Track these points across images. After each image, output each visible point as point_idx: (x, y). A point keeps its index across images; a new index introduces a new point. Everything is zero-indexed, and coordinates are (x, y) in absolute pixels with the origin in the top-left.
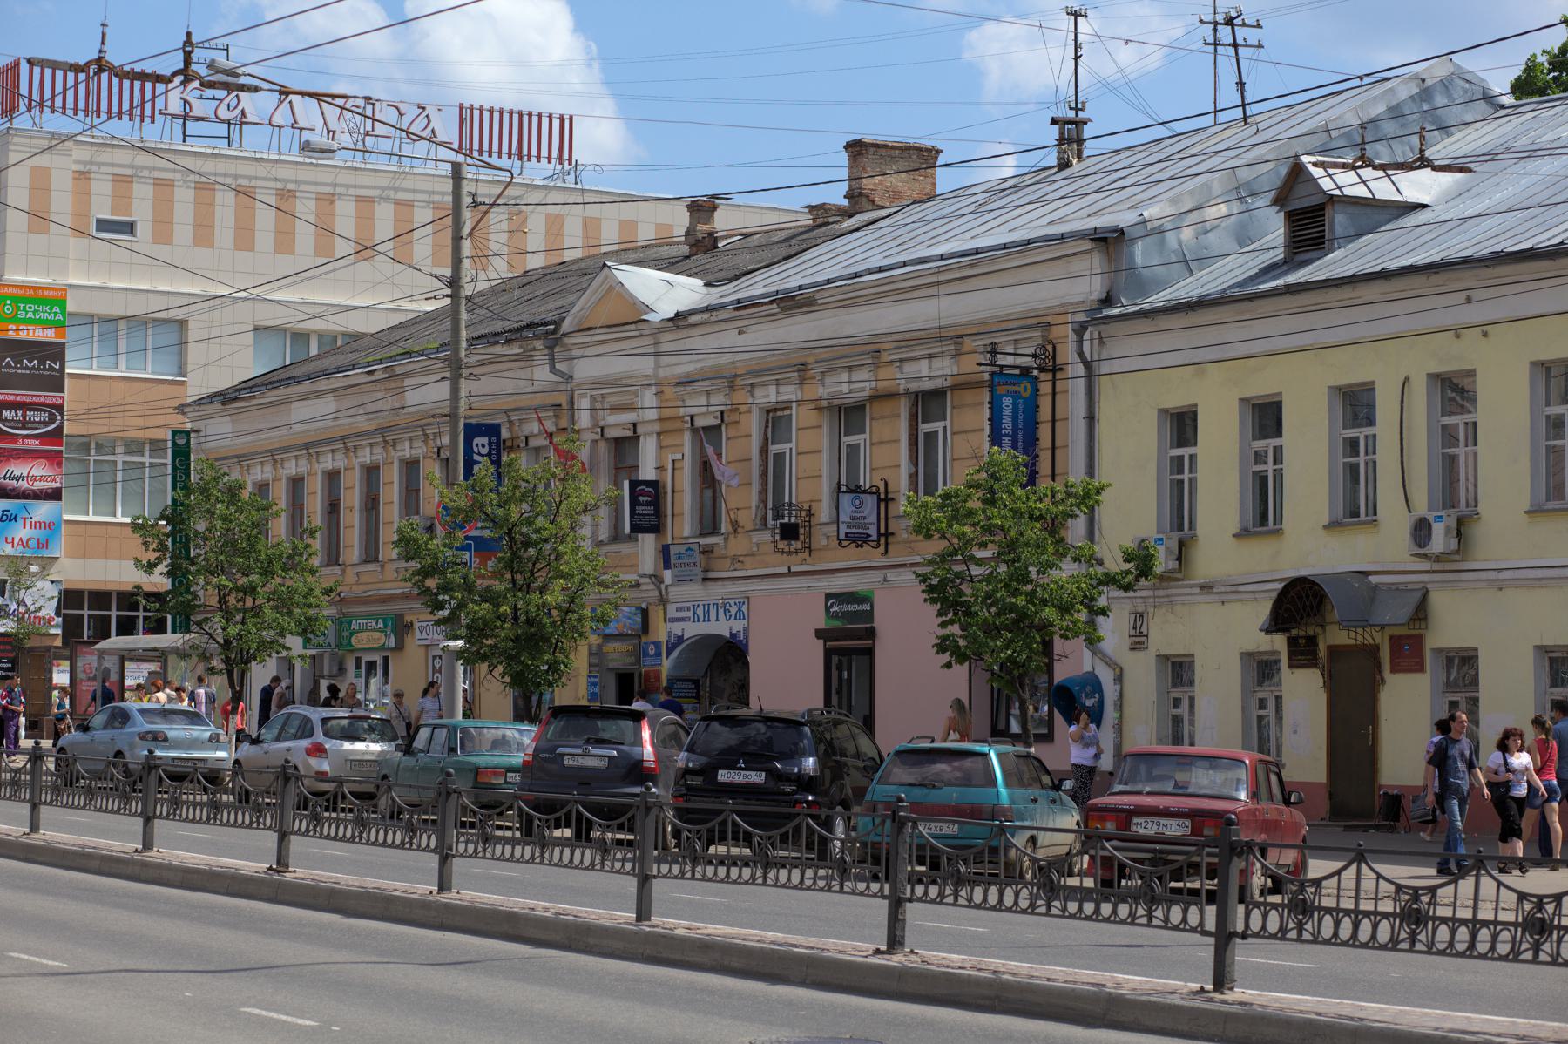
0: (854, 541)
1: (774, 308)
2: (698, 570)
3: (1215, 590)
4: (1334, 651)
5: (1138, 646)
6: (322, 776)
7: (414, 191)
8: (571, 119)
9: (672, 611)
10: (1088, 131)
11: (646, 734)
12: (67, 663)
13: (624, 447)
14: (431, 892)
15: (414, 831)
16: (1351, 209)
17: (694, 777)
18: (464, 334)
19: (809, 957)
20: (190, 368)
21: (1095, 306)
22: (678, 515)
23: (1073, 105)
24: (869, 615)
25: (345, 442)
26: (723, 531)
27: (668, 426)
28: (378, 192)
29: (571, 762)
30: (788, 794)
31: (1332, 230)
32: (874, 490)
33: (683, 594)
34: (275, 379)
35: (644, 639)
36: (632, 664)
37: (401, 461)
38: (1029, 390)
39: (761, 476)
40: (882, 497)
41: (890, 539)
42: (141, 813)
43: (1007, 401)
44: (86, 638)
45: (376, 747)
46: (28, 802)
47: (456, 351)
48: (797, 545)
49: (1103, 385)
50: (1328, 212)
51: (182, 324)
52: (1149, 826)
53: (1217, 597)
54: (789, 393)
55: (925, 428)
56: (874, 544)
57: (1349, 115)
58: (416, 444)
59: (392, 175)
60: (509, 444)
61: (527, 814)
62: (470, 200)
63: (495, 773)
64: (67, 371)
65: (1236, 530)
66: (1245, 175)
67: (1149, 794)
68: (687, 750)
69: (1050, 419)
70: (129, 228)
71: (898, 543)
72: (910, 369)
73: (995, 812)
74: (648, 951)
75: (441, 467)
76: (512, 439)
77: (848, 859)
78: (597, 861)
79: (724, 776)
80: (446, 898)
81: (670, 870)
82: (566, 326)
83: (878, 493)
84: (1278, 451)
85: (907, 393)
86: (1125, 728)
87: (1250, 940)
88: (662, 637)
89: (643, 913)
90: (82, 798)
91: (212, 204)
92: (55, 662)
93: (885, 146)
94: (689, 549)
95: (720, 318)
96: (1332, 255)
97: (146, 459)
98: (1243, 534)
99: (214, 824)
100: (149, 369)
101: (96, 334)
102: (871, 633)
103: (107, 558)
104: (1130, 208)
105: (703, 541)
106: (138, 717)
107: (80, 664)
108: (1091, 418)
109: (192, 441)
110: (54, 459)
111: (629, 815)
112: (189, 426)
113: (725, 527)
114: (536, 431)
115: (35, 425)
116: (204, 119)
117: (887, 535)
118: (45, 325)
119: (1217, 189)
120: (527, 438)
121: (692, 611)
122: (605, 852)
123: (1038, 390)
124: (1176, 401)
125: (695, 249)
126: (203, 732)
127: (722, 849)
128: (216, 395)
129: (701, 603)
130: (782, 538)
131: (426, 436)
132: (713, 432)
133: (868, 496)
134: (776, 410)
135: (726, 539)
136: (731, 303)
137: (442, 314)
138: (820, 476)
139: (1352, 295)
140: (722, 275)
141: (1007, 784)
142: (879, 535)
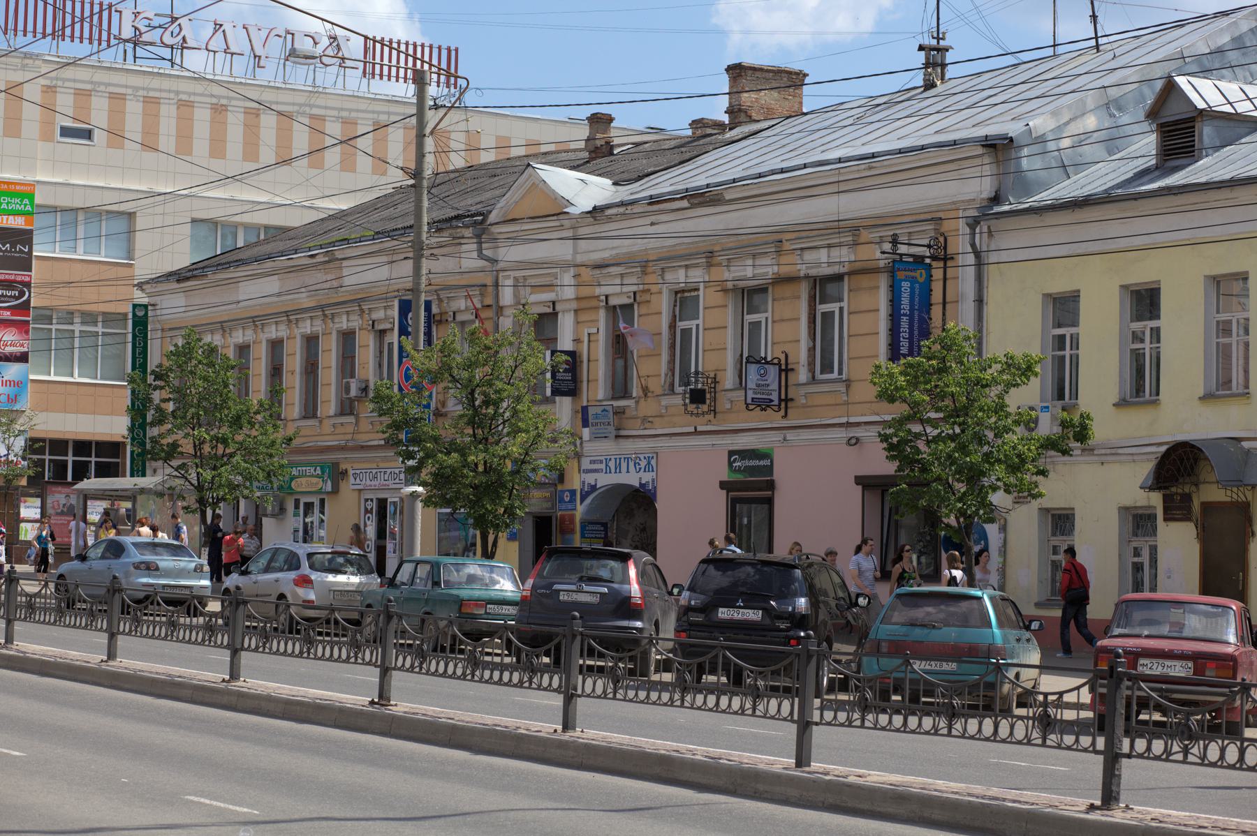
0: (759, 406)
1: (685, 203)
2: (611, 429)
3: (1095, 452)
4: (1206, 506)
5: (1021, 500)
6: (308, 604)
7: (326, 108)
8: (457, 50)
9: (586, 464)
10: (949, 57)
11: (632, 572)
12: (38, 502)
13: (546, 322)
14: (555, 731)
15: (358, 647)
16: (1216, 123)
17: (695, 614)
18: (425, 220)
19: (1028, 812)
20: (137, 254)
21: (985, 203)
22: (593, 381)
23: (935, 35)
24: (769, 470)
25: (290, 316)
26: (634, 395)
27: (584, 304)
28: (296, 108)
29: (566, 598)
30: (782, 630)
31: (1201, 140)
32: (776, 361)
33: (596, 448)
34: (224, 261)
35: (560, 487)
36: (547, 509)
37: (338, 332)
38: (924, 276)
39: (670, 348)
40: (783, 367)
41: (790, 404)
42: (228, 644)
43: (906, 285)
44: (46, 479)
45: (355, 579)
46: (105, 631)
47: (419, 234)
48: (705, 408)
49: (991, 272)
50: (1198, 126)
51: (131, 216)
52: (1154, 667)
53: (1096, 458)
54: (697, 275)
55: (823, 308)
56: (776, 408)
57: (1200, 43)
58: (352, 317)
59: (307, 94)
60: (438, 318)
61: (736, 664)
62: (432, 103)
63: (476, 605)
64: (34, 254)
65: (1116, 400)
66: (1113, 92)
67: (1147, 637)
68: (688, 590)
69: (941, 301)
70: (88, 134)
71: (797, 407)
72: (808, 256)
73: (991, 651)
74: (831, 801)
75: (375, 337)
76: (441, 314)
77: (425, 647)
78: (609, 690)
79: (724, 613)
80: (1117, 816)
81: (659, 698)
82: (492, 218)
83: (779, 364)
84: (1156, 333)
85: (807, 277)
86: (1009, 571)
87: (1133, 760)
88: (577, 486)
89: (802, 759)
90: (84, 619)
91: (157, 116)
92: (22, 499)
93: (761, 70)
94: (604, 410)
95: (635, 211)
96: (1201, 162)
97: (99, 329)
98: (1122, 404)
99: (208, 646)
100: (103, 253)
101: (58, 223)
102: (771, 485)
103: (65, 412)
104: (1013, 119)
105: (616, 403)
106: (132, 549)
107: (49, 501)
108: (980, 301)
109: (150, 313)
110: (23, 327)
111: (556, 641)
112: (145, 301)
113: (636, 391)
114: (463, 307)
115: (6, 299)
116: (151, 44)
117: (787, 400)
118: (16, 214)
119: (1090, 104)
120: (454, 313)
121: (605, 464)
122: (616, 682)
123: (931, 276)
124: (1060, 286)
125: (594, 155)
126: (188, 563)
127: (712, 678)
128: (171, 274)
129: (613, 457)
130: (692, 402)
131: (362, 311)
132: (628, 308)
133: (771, 366)
134: (683, 291)
135: (637, 402)
136: (644, 198)
137: (367, 208)
138: (725, 349)
139: (1230, 196)
140: (625, 176)
141: (1001, 624)
142: (780, 400)
